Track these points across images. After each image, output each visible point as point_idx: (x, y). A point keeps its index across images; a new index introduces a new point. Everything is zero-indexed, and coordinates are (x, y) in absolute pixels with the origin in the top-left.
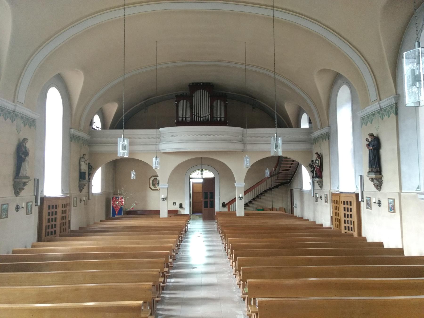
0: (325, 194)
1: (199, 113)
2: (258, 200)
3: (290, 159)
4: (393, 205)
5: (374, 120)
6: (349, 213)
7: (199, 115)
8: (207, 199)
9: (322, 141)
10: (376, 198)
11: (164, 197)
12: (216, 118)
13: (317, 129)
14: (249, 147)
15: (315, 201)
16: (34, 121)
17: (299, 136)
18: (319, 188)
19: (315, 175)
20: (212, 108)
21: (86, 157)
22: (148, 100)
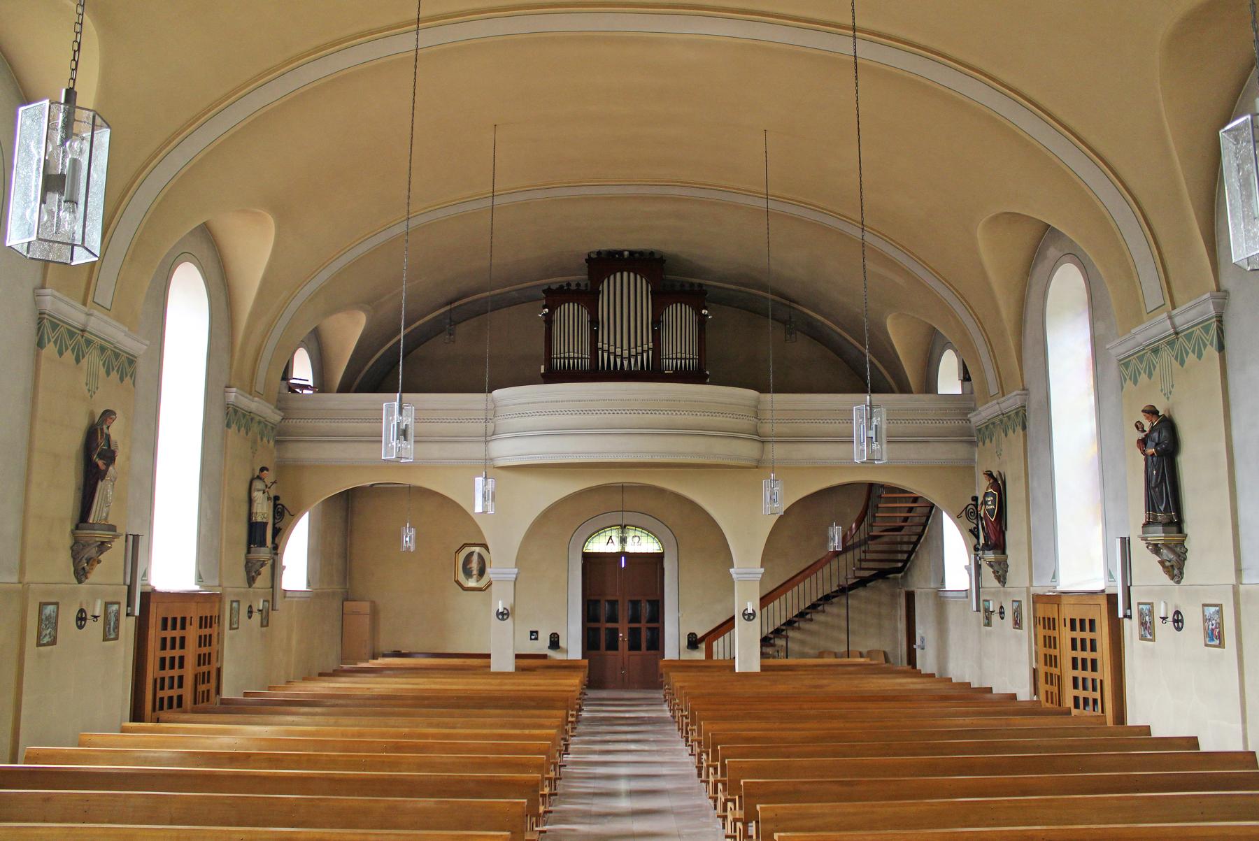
0: (1014, 601)
1: (618, 344)
2: (803, 625)
3: (904, 491)
4: (1219, 624)
5: (1158, 366)
6: (1088, 655)
7: (619, 351)
8: (639, 622)
10: (1166, 604)
11: (505, 609)
12: (671, 361)
13: (987, 398)
14: (777, 452)
15: (982, 624)
16: (132, 361)
18: (996, 583)
19: (982, 541)
20: (659, 329)
21: (269, 477)
22: (456, 304)
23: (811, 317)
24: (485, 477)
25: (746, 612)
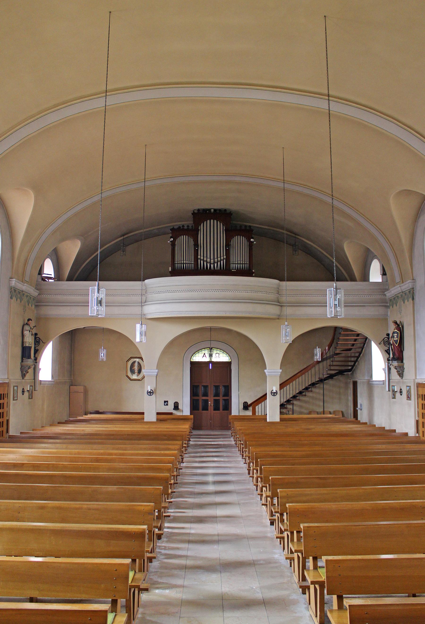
0: (407, 386)
1: (208, 257)
2: (301, 398)
3: (354, 331)
8: (219, 396)
9: (402, 303)
11: (151, 390)
12: (235, 265)
13: (395, 284)
14: (288, 311)
15: (391, 398)
17: (368, 295)
18: (398, 377)
19: (391, 356)
20: (229, 248)
21: (32, 323)
23: (306, 243)
24: (141, 324)
25: (272, 392)
